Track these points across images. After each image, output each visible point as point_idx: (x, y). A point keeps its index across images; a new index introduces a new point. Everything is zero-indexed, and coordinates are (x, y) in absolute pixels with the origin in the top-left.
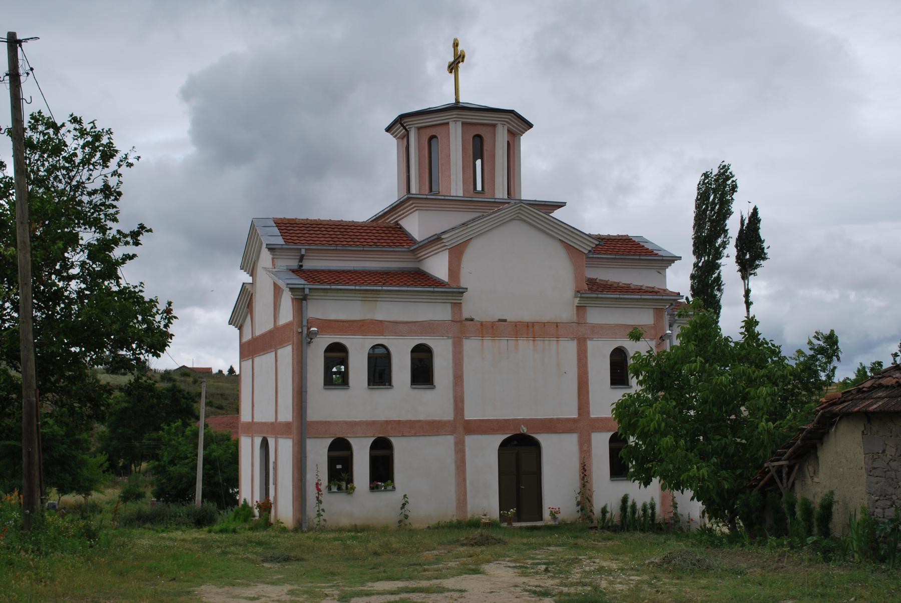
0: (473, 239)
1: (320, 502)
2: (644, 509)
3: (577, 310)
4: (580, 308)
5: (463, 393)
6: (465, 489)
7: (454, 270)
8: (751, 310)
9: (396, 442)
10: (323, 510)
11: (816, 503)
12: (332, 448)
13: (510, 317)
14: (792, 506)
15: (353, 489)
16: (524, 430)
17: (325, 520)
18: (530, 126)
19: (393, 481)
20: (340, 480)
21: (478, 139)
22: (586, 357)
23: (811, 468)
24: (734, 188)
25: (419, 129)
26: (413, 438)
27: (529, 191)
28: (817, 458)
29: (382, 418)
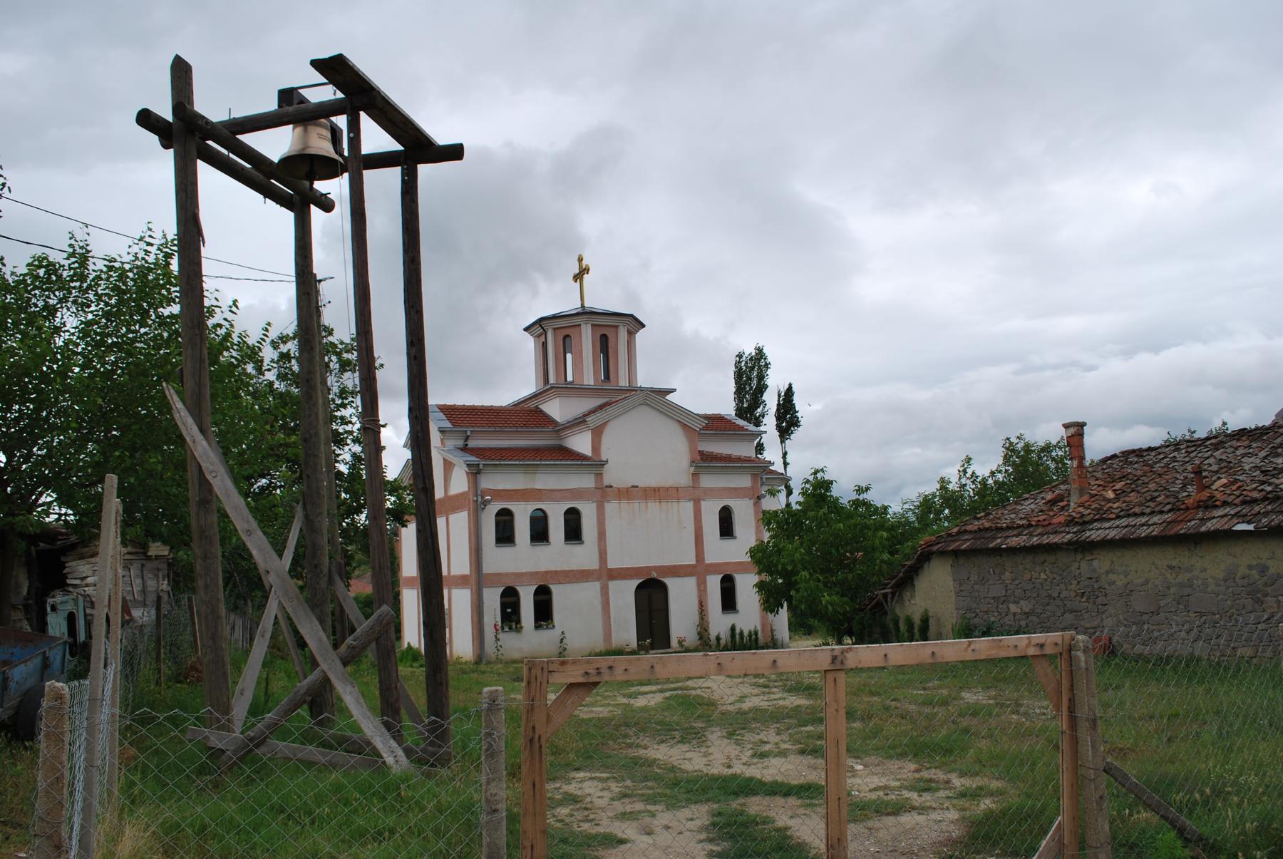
0: (609, 423)
1: (498, 640)
2: (750, 635)
3: (693, 477)
4: (695, 475)
6: (610, 625)
8: (788, 469)
10: (501, 646)
11: (917, 620)
12: (503, 595)
13: (640, 484)
14: (896, 622)
15: (521, 628)
16: (654, 575)
18: (643, 326)
19: (552, 621)
20: (511, 621)
21: (604, 339)
22: (701, 515)
23: (908, 594)
24: (767, 365)
25: (555, 329)
27: (645, 379)
28: (914, 586)
29: (543, 569)
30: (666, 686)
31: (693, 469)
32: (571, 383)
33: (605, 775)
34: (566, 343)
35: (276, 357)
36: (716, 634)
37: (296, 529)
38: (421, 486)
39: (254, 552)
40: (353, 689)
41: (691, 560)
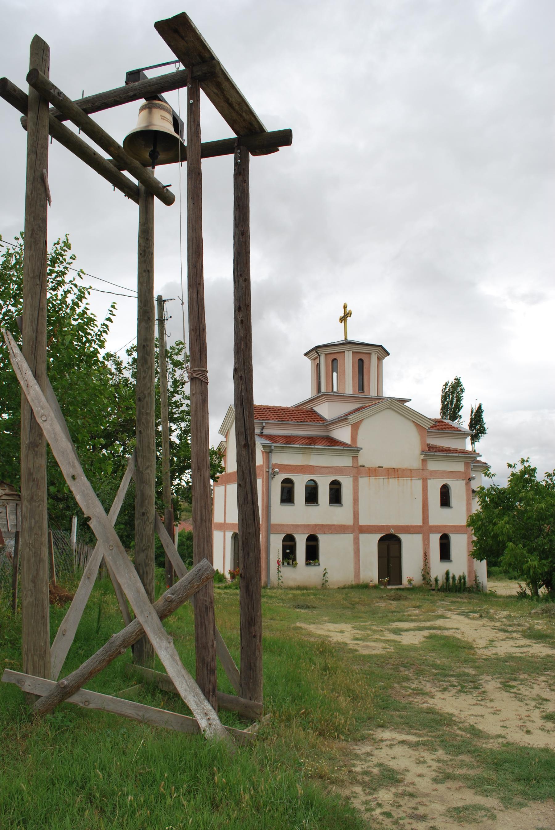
1: (279, 571)
2: (460, 579)
5: (358, 509)
6: (359, 565)
7: (354, 437)
9: (320, 537)
10: (281, 576)
15: (296, 564)
16: (392, 531)
17: (282, 582)
18: (388, 354)
20: (289, 559)
22: (427, 489)
24: (462, 391)
25: (326, 354)
26: (330, 535)
30: (422, 624)
31: (422, 457)
32: (335, 392)
33: (412, 738)
34: (334, 364)
35: (131, 361)
36: (435, 577)
37: (126, 479)
38: (243, 443)
39: (78, 498)
40: (169, 645)
41: (420, 523)
